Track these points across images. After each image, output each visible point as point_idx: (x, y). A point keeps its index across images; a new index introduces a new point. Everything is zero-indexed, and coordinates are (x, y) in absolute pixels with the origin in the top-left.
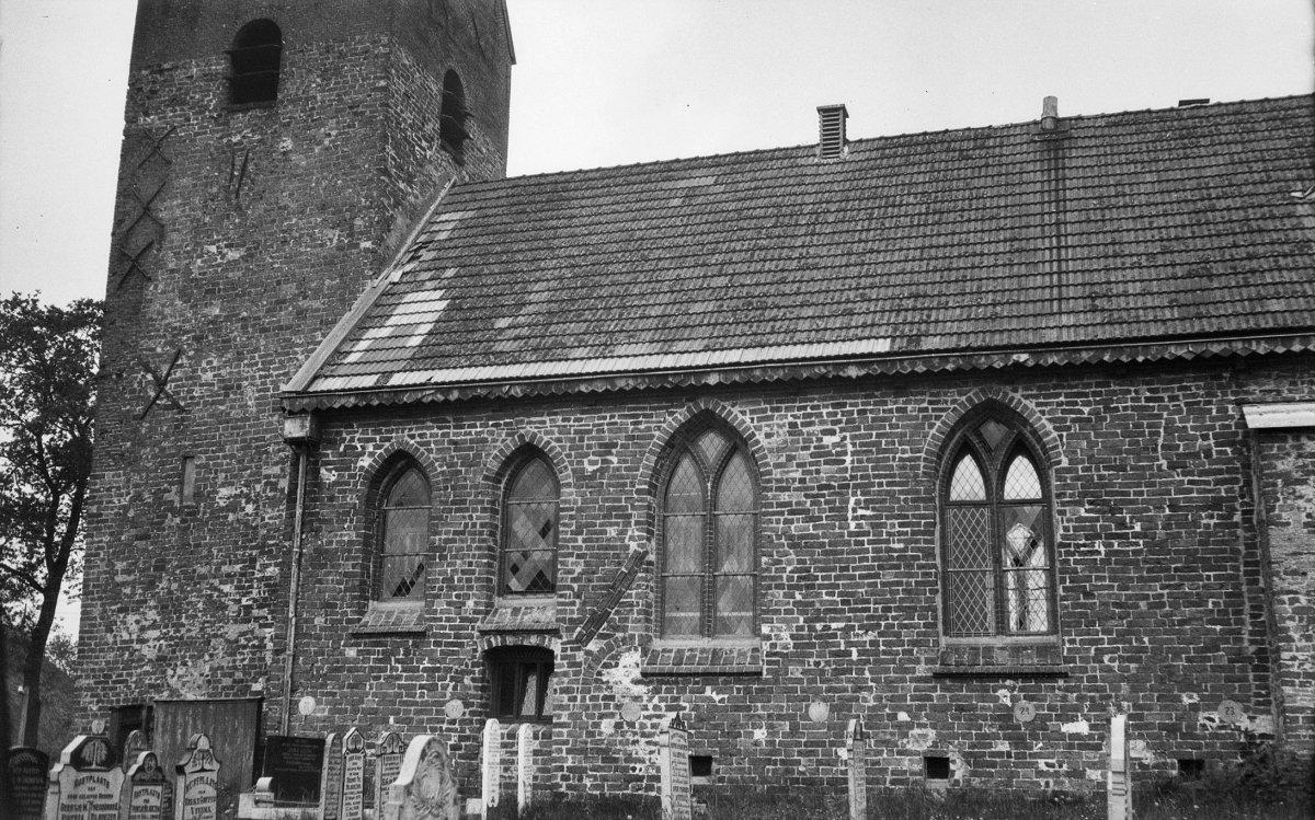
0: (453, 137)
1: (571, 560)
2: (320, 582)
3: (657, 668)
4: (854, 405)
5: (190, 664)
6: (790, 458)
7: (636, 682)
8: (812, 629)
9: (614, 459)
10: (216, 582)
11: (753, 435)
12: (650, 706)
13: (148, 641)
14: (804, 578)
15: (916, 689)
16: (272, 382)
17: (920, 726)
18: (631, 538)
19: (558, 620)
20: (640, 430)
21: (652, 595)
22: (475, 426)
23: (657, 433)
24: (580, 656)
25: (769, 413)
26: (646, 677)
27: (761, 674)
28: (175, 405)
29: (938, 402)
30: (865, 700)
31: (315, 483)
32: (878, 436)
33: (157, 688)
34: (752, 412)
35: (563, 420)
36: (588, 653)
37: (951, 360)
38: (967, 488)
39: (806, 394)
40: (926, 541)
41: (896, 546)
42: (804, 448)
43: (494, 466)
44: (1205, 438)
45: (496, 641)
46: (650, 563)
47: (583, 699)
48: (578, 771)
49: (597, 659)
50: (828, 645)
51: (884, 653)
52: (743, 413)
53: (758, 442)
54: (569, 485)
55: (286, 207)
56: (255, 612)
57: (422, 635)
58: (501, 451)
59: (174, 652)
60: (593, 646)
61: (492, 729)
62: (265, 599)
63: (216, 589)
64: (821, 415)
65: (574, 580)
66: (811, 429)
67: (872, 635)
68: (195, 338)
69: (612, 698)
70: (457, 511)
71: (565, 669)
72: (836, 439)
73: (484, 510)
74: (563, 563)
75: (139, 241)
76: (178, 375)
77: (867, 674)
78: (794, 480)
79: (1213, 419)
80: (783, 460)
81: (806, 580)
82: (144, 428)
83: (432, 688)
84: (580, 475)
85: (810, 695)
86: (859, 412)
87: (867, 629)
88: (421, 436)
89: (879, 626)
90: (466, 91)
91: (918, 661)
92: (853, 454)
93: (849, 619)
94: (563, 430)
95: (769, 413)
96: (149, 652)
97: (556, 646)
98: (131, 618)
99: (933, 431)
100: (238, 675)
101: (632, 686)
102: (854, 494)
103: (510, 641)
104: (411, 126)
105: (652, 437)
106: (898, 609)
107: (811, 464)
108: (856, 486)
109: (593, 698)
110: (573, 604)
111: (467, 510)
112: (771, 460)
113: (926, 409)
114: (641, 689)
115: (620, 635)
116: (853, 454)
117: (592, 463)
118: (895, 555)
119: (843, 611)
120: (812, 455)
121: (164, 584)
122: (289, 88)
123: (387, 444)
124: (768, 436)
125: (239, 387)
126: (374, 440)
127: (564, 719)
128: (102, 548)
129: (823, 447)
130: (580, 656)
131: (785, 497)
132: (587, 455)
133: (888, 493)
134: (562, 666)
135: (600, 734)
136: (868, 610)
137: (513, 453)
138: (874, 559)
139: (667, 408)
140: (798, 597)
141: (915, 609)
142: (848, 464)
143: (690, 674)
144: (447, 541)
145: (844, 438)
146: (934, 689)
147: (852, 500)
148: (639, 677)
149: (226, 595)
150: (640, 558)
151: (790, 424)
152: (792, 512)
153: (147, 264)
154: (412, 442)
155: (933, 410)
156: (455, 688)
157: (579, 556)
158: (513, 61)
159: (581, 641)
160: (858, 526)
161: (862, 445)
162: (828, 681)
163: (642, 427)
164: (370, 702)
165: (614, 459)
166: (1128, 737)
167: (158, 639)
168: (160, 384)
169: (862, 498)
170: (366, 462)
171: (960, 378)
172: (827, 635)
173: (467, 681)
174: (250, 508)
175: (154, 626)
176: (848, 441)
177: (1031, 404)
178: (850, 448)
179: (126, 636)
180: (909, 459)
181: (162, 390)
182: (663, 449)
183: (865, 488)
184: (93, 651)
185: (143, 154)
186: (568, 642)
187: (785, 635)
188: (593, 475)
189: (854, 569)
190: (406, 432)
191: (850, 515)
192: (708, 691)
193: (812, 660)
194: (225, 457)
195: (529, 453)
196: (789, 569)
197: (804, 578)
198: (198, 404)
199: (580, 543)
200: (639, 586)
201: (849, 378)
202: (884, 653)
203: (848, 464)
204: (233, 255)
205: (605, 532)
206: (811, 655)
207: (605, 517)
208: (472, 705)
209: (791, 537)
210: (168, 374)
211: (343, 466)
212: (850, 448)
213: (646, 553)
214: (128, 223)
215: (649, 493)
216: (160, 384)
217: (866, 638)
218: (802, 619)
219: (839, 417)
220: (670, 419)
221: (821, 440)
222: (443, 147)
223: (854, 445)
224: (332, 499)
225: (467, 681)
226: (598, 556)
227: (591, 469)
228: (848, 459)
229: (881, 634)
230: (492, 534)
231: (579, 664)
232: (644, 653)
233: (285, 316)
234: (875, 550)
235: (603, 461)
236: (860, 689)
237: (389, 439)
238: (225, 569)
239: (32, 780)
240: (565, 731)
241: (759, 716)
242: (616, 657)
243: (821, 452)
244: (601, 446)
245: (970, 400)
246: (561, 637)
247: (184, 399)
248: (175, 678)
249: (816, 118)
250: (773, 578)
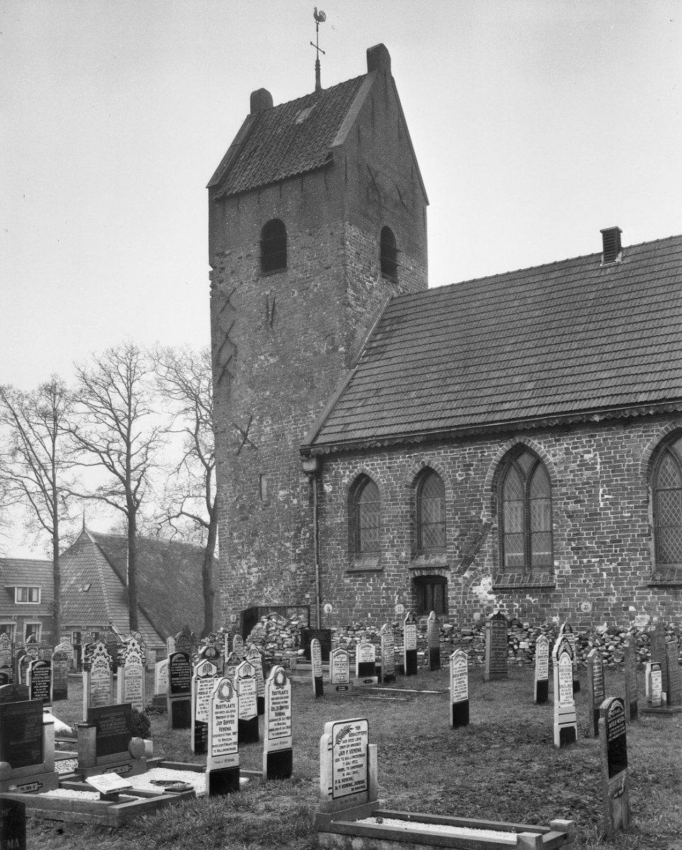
0: (389, 268)
1: (453, 529)
2: (328, 544)
3: (500, 585)
4: (601, 436)
5: (274, 584)
6: (566, 468)
7: (490, 593)
8: (581, 562)
9: (472, 473)
11: (546, 455)
12: (498, 605)
13: (252, 574)
14: (577, 535)
15: (639, 594)
16: (300, 431)
17: (642, 613)
18: (484, 516)
19: (448, 561)
20: (485, 456)
21: (496, 546)
22: (399, 458)
23: (494, 457)
24: (460, 580)
25: (554, 443)
26: (495, 590)
27: (555, 587)
28: (253, 446)
29: (648, 431)
30: (611, 600)
31: (323, 493)
32: (614, 453)
33: (260, 597)
34: (545, 442)
35: (445, 452)
36: (465, 578)
37: (652, 408)
38: (318, 648)
39: (575, 430)
40: (643, 512)
41: (626, 515)
42: (573, 462)
43: (410, 480)
45: (417, 573)
46: (495, 529)
47: (464, 603)
49: (469, 581)
50: (590, 571)
51: (621, 574)
52: (540, 443)
53: (548, 459)
54: (449, 488)
57: (381, 571)
58: (413, 471)
59: (266, 579)
60: (467, 575)
62: (307, 550)
63: (283, 545)
64: (582, 442)
65: (455, 540)
66: (576, 451)
67: (614, 564)
69: (478, 601)
70: (393, 504)
71: (454, 587)
72: (591, 456)
73: (406, 504)
74: (449, 531)
75: (225, 356)
76: (253, 430)
77: (612, 586)
78: (569, 480)
80: (562, 468)
81: (577, 536)
84: (454, 481)
86: (604, 439)
87: (611, 562)
88: (372, 465)
89: (618, 559)
90: (396, 236)
92: (601, 464)
93: (601, 557)
94: (445, 458)
95: (554, 443)
96: (253, 579)
97: (448, 575)
98: (244, 562)
99: (646, 448)
101: (488, 595)
102: (602, 486)
103: (424, 573)
104: (362, 271)
105: (492, 459)
106: (628, 550)
107: (578, 470)
108: (603, 482)
109: (469, 602)
110: (455, 552)
111: (398, 504)
112: (555, 469)
113: (641, 436)
114: (492, 597)
115: (480, 568)
116: (601, 464)
117: (460, 475)
118: (626, 520)
119: (597, 552)
120: (578, 466)
122: (292, 260)
123: (356, 470)
125: (283, 435)
126: (348, 468)
127: (455, 613)
128: (225, 525)
129: (584, 460)
130: (460, 580)
131: (564, 490)
132: (458, 471)
133: (621, 485)
134: (451, 585)
135: (474, 620)
136: (611, 551)
137: (419, 472)
138: (614, 523)
139: (498, 443)
140: (574, 545)
141: (637, 550)
142: (598, 470)
143: (518, 588)
144: (390, 521)
145: (596, 455)
146: (649, 593)
147: (601, 490)
148: (492, 590)
149: (288, 548)
150: (487, 526)
151: (565, 448)
152: (568, 498)
153: (230, 369)
154: (368, 468)
155: (646, 436)
156: (399, 598)
157: (457, 527)
158: (427, 203)
159: (460, 572)
160: (605, 504)
161: (605, 458)
162: (591, 590)
163: (486, 454)
165: (472, 473)
167: (258, 572)
168: (245, 435)
169: (607, 489)
170: (346, 481)
171: (661, 416)
173: (405, 594)
174: (295, 501)
175: (255, 565)
176: (598, 456)
178: (599, 460)
179: (242, 571)
180: (632, 465)
181: (246, 439)
182: (498, 466)
183: (608, 483)
184: (227, 579)
185: (221, 304)
186: (454, 573)
187: (567, 567)
188: (461, 482)
189: (603, 529)
190: (365, 463)
191: (600, 498)
192: (528, 597)
193: (582, 579)
194: (280, 474)
195: (427, 473)
196: (568, 530)
197: (577, 535)
198: (264, 445)
199: (457, 520)
200: (489, 542)
201: (595, 422)
202: (621, 574)
203: (598, 470)
204: (272, 360)
205: (469, 513)
206: (581, 576)
207: (469, 505)
208: (408, 606)
209: (567, 512)
210: (248, 430)
212: (599, 460)
213: (492, 523)
214: (219, 344)
215: (492, 490)
217: (611, 567)
218: (576, 558)
219: (593, 443)
220: (500, 449)
221: (582, 456)
222: (383, 277)
223: (601, 459)
224: (331, 500)
225: (405, 594)
226: (466, 526)
227: (460, 479)
228: (598, 467)
229: (619, 564)
230: (411, 516)
231: (461, 584)
232: (494, 578)
234: (615, 518)
235: (467, 474)
236: (608, 594)
237: (356, 467)
239: (184, 664)
240: (455, 619)
241: (555, 610)
242: (479, 580)
243: (583, 464)
244: (464, 466)
245: (667, 429)
246: (450, 570)
247: (257, 443)
248: (268, 593)
249: (601, 234)
250: (560, 535)
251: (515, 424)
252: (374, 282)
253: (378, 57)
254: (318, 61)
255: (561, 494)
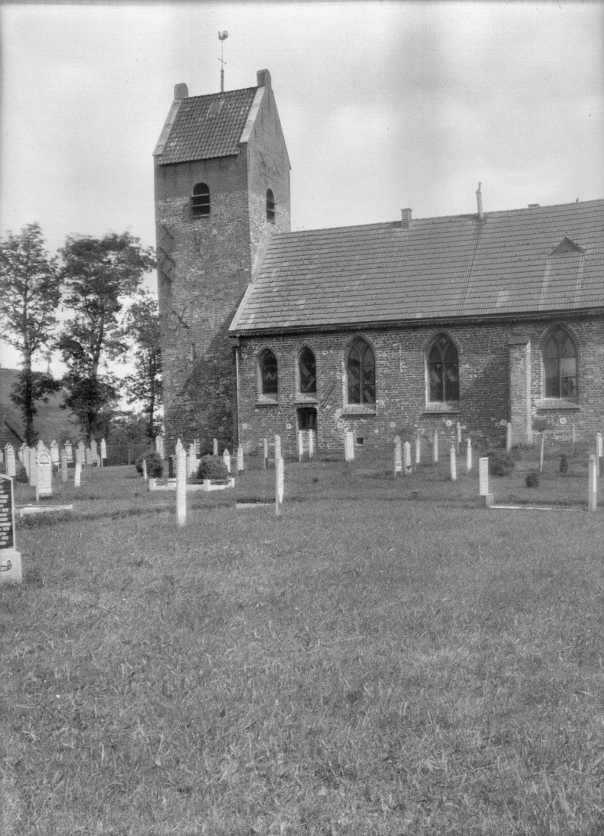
4: (402, 334)
8: (390, 401)
10: (207, 386)
36: (327, 409)
44: (501, 344)
48: (325, 443)
55: (217, 255)
56: (221, 396)
61: (301, 433)
67: (407, 403)
68: (190, 302)
79: (504, 338)
82: (177, 333)
83: (282, 420)
85: (391, 420)
91: (420, 410)
96: (187, 408)
97: (317, 407)
100: (218, 415)
103: (304, 406)
121: (190, 386)
124: (377, 344)
130: (324, 410)
131: (382, 362)
164: (264, 425)
166: (263, 447)
168: (180, 319)
170: (256, 352)
172: (394, 403)
175: (188, 400)
177: (453, 334)
187: (383, 404)
204: (201, 272)
209: (383, 374)
211: (249, 354)
216: (180, 319)
227: (325, 354)
233: (221, 295)
238: (210, 381)
242: (335, 410)
251: (544, 511)
252: (266, 225)
253: (264, 77)
254: (222, 71)
255: (381, 365)
